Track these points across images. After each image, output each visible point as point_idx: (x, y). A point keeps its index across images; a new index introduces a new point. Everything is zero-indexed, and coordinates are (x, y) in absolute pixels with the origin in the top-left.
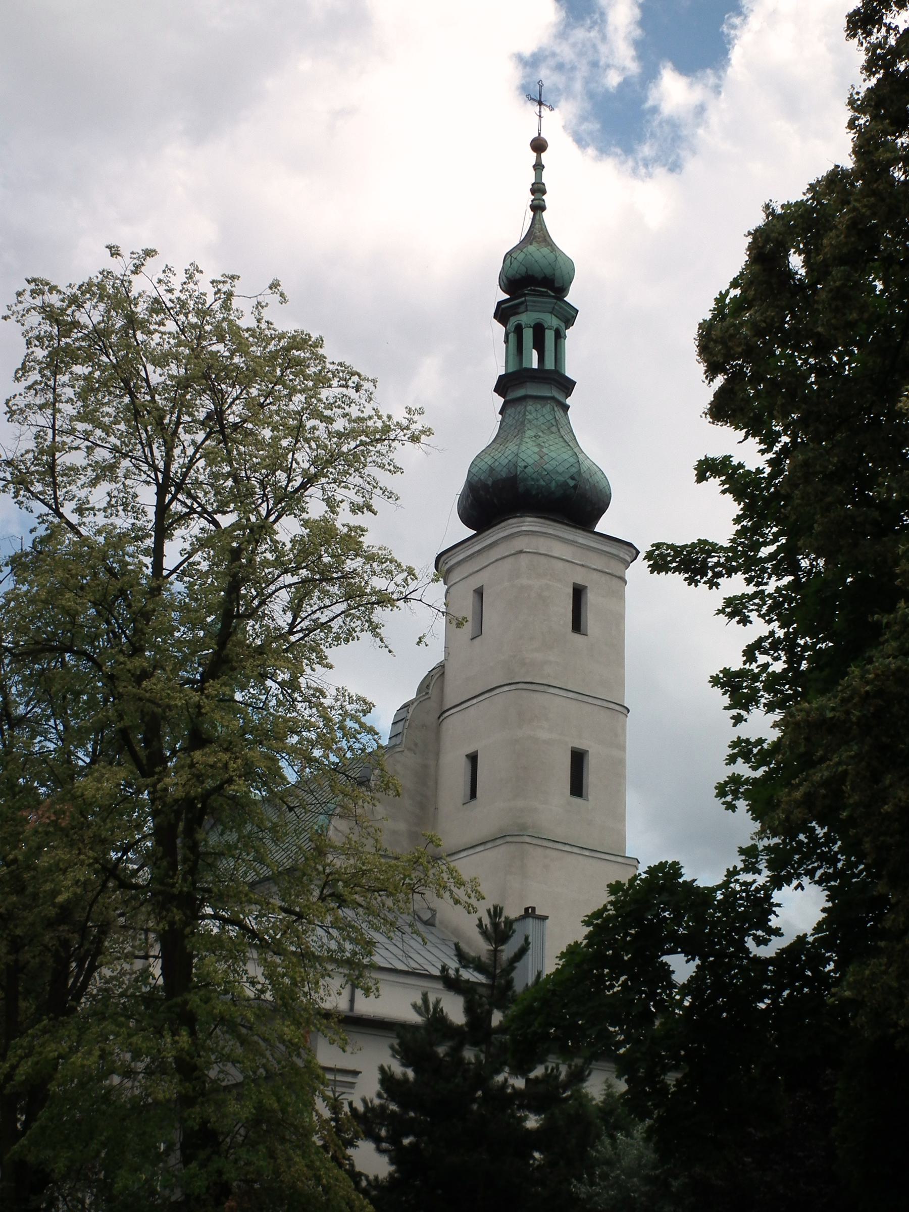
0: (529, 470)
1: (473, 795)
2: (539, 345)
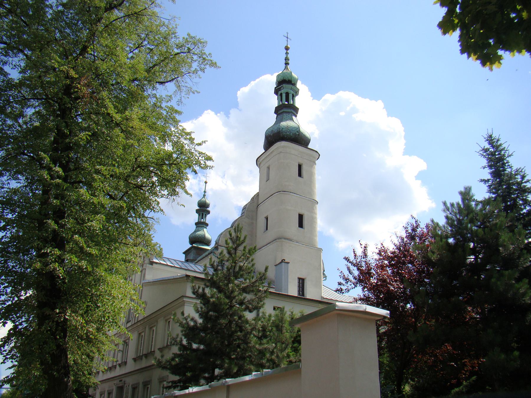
0: (284, 130)
1: (267, 229)
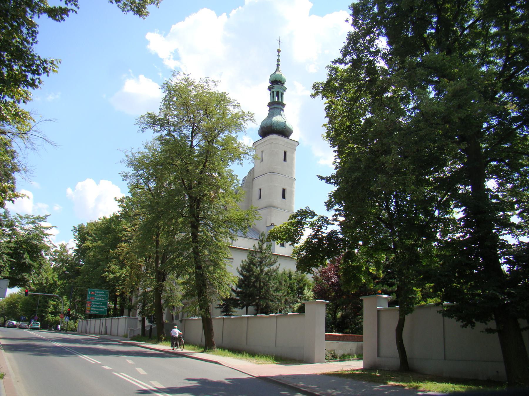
1: (260, 198)
2: (278, 96)
